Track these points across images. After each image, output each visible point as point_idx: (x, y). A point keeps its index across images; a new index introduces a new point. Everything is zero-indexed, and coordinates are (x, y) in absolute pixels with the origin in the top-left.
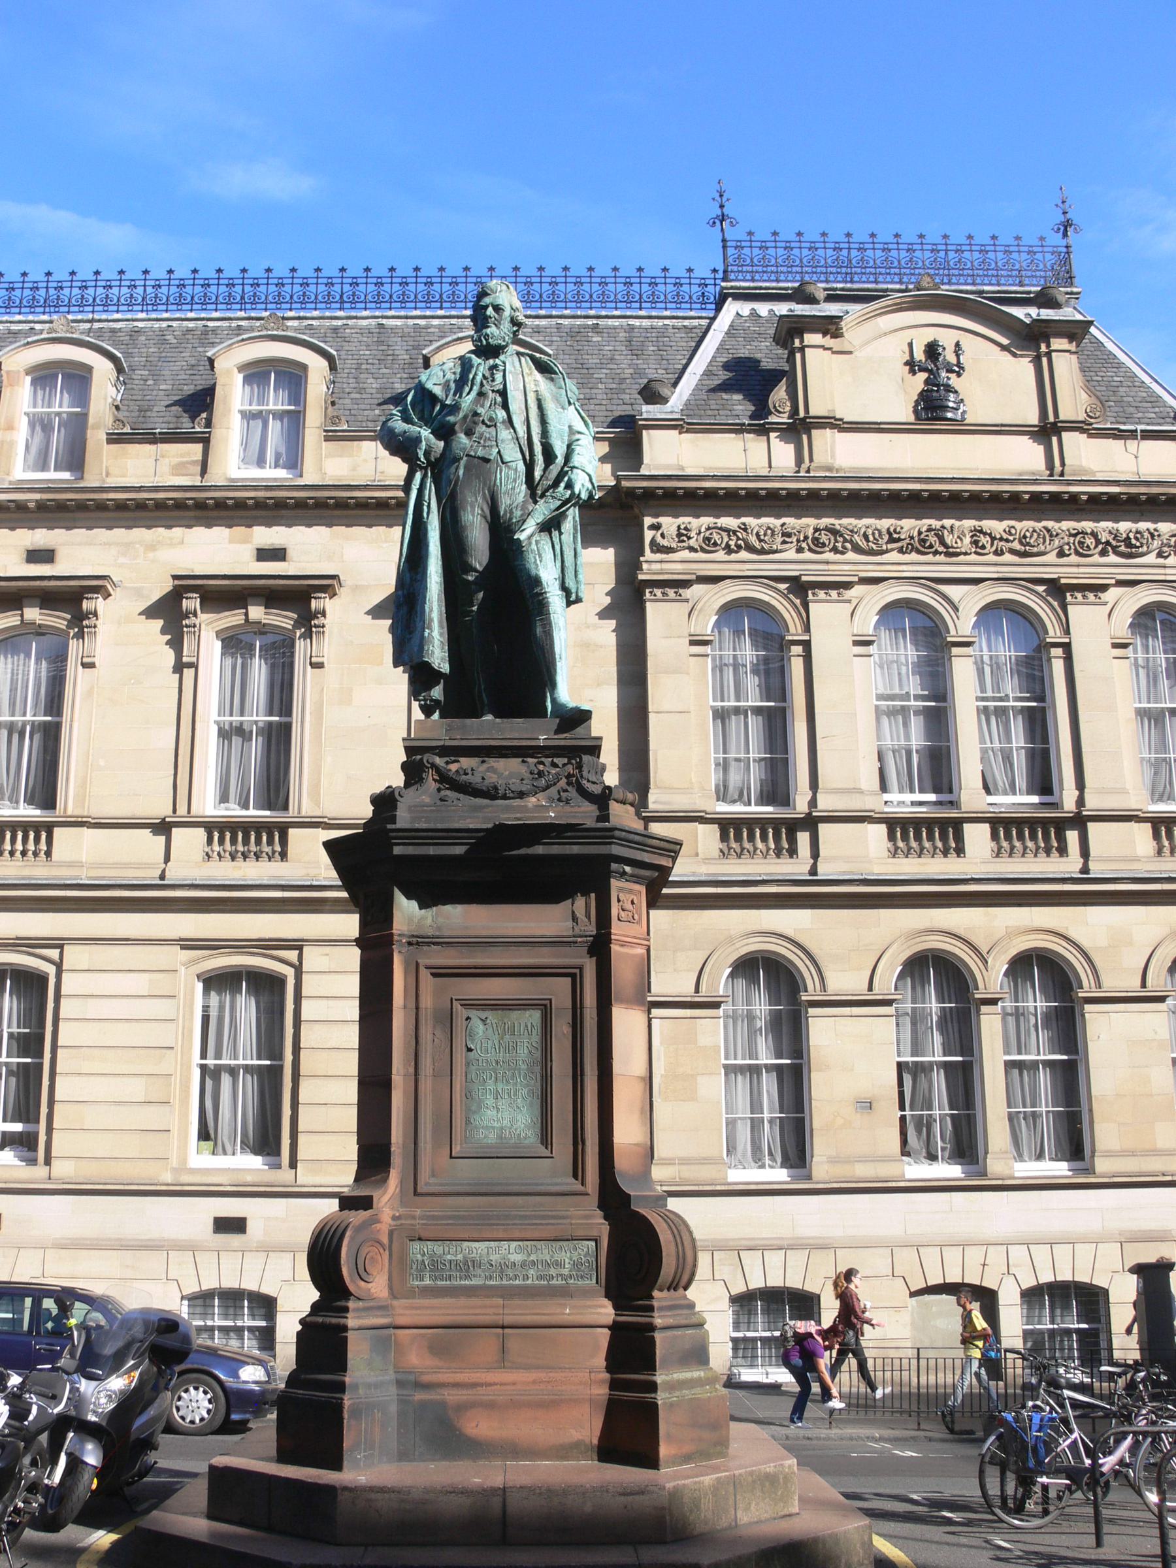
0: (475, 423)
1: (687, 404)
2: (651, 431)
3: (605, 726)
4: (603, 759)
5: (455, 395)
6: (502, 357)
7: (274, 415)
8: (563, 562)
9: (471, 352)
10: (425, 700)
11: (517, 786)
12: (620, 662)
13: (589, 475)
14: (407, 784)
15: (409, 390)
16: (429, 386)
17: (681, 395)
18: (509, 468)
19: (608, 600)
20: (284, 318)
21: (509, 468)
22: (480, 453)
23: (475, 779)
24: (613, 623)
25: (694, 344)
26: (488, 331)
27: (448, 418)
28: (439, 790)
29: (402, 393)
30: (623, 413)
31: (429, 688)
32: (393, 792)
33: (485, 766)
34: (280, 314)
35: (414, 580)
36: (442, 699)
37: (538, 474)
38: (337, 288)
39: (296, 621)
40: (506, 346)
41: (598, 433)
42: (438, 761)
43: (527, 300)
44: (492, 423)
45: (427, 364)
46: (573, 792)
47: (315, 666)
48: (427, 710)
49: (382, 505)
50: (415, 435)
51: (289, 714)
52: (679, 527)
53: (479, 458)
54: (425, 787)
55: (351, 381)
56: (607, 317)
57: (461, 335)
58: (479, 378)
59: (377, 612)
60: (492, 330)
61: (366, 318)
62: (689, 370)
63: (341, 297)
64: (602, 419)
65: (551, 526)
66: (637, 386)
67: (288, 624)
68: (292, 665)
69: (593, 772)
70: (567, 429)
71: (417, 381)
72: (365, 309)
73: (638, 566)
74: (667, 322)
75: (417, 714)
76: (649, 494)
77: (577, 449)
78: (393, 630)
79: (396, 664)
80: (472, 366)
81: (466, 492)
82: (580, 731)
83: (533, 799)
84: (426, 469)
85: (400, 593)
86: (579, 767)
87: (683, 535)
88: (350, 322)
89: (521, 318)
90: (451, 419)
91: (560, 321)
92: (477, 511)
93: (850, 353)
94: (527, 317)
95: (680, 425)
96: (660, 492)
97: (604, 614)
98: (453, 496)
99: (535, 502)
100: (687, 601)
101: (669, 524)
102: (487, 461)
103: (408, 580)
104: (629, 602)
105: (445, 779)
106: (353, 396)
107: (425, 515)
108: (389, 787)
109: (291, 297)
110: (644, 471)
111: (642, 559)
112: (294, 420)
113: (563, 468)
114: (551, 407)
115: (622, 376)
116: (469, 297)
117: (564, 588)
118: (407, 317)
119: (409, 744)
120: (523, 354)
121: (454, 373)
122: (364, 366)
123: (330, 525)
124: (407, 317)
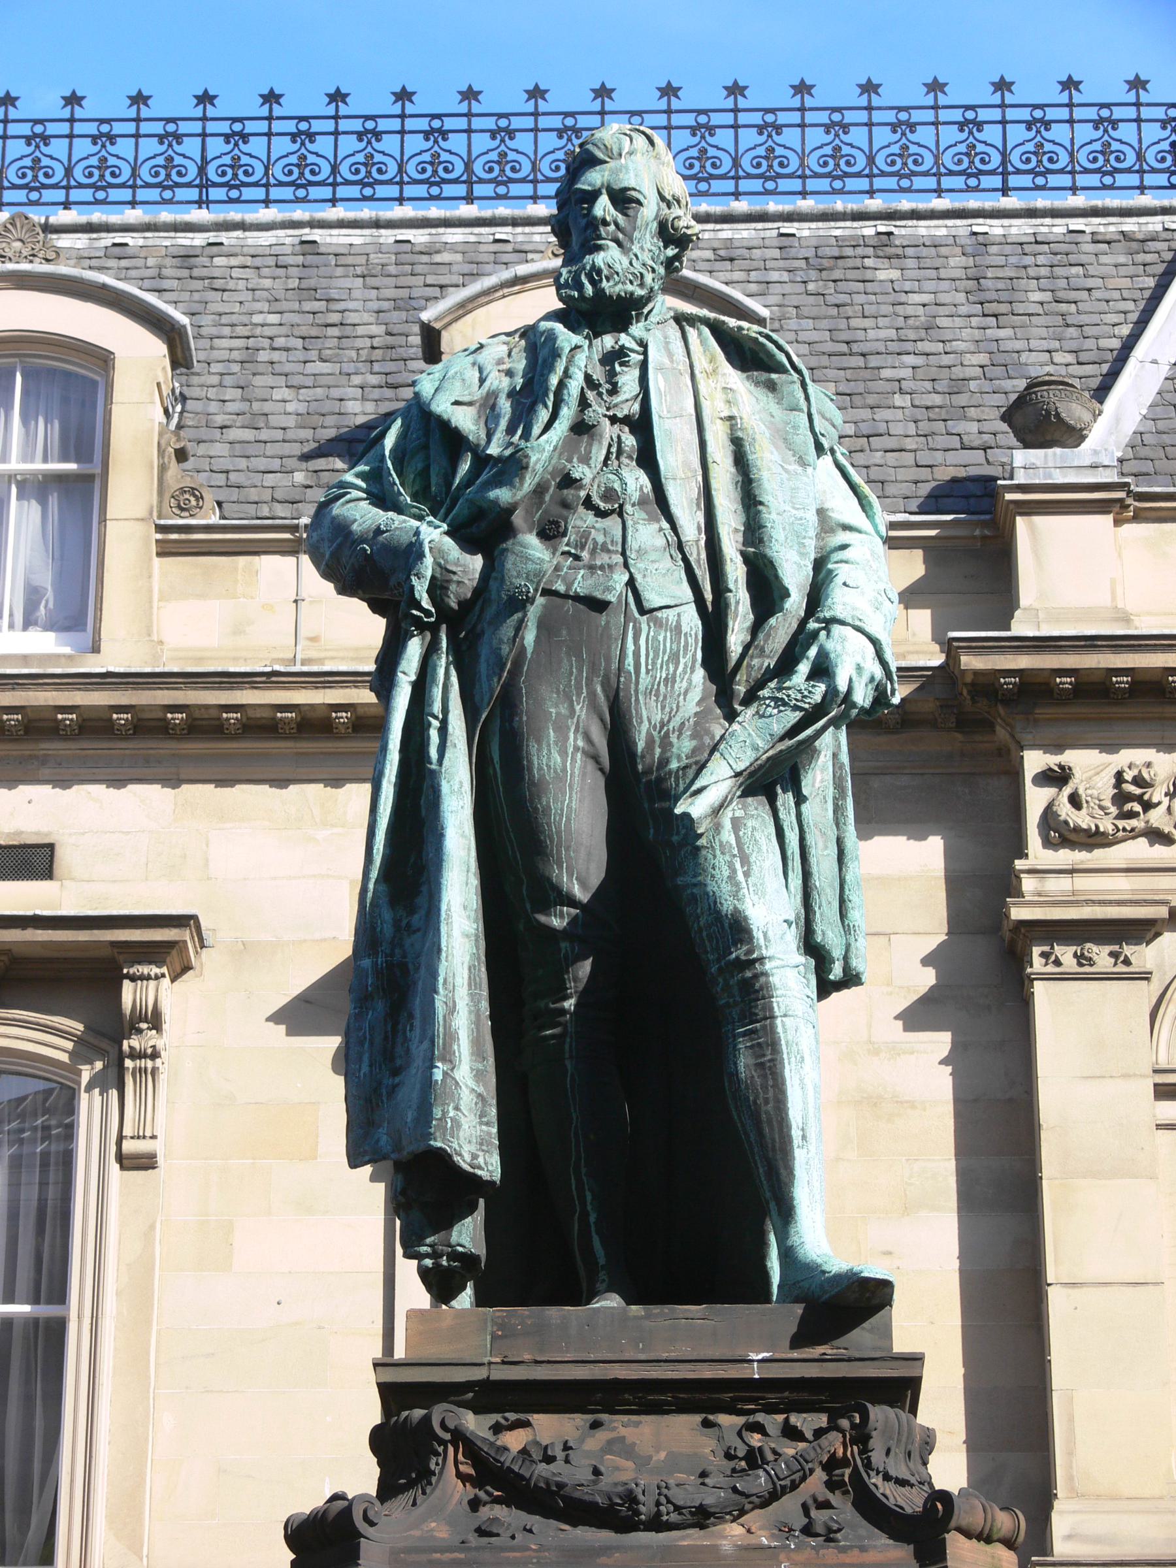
0: (566, 505)
1: (1137, 442)
2: (1037, 519)
3: (928, 1324)
4: (926, 1416)
5: (511, 431)
6: (637, 329)
7: (21, 485)
8: (806, 875)
9: (549, 316)
10: (435, 1255)
11: (690, 1494)
12: (963, 1149)
13: (874, 642)
14: (387, 1489)
15: (386, 419)
16: (442, 407)
17: (1117, 420)
18: (659, 624)
19: (928, 978)
20: (48, 228)
21: (659, 624)
22: (581, 584)
23: (573, 1474)
24: (942, 1041)
25: (1151, 282)
26: (599, 259)
27: (493, 494)
28: (475, 1504)
29: (368, 427)
30: (962, 473)
31: (447, 1223)
32: (347, 1512)
33: (602, 1436)
34: (37, 216)
35: (402, 929)
36: (480, 1250)
37: (736, 640)
38: (191, 147)
39: (80, 1041)
40: (649, 299)
41: (893, 526)
42: (472, 1422)
43: (699, 172)
44: (611, 506)
45: (432, 350)
46: (844, 1509)
47: (128, 1162)
48: (441, 1285)
49: (314, 725)
50: (406, 539)
51: (60, 1295)
52: (1119, 776)
53: (577, 598)
54: (435, 1496)
55: (230, 394)
56: (915, 215)
57: (522, 270)
58: (575, 385)
59: (299, 1016)
60: (609, 256)
61: (267, 228)
62: (1140, 351)
63: (202, 170)
64: (908, 489)
65: (772, 779)
66: (999, 400)
67: (58, 1050)
68: (67, 1161)
69: (898, 1452)
70: (812, 518)
71: (407, 393)
72: (267, 202)
73: (1009, 886)
74: (1077, 224)
75: (413, 1294)
76: (1034, 692)
77: (842, 573)
78: (345, 1062)
79: (355, 1159)
80: (555, 354)
81: (544, 690)
82: (860, 1338)
83: (735, 1530)
84: (434, 629)
85: (366, 963)
86: (861, 1437)
87: (1130, 798)
88: (224, 237)
89: (685, 222)
90: (503, 495)
91: (788, 228)
92: (574, 740)
93: (1159, 1127)
94: (701, 218)
95: (1118, 502)
96: (1066, 681)
97: (917, 1017)
98: (508, 702)
99: (731, 716)
100: (1145, 977)
101: (1093, 768)
102: (600, 606)
103: (388, 931)
104: (988, 982)
105: (493, 1477)
106: (234, 434)
107: (433, 753)
108: (336, 1497)
109: (69, 172)
110: (1021, 627)
111: (1019, 864)
112: (77, 494)
113: (803, 623)
114: (768, 461)
115: (958, 372)
116: (545, 167)
117: (812, 948)
118: (377, 224)
119: (391, 1376)
120: (692, 320)
121: (509, 373)
122: (263, 356)
123: (173, 782)
124: (377, 224)
